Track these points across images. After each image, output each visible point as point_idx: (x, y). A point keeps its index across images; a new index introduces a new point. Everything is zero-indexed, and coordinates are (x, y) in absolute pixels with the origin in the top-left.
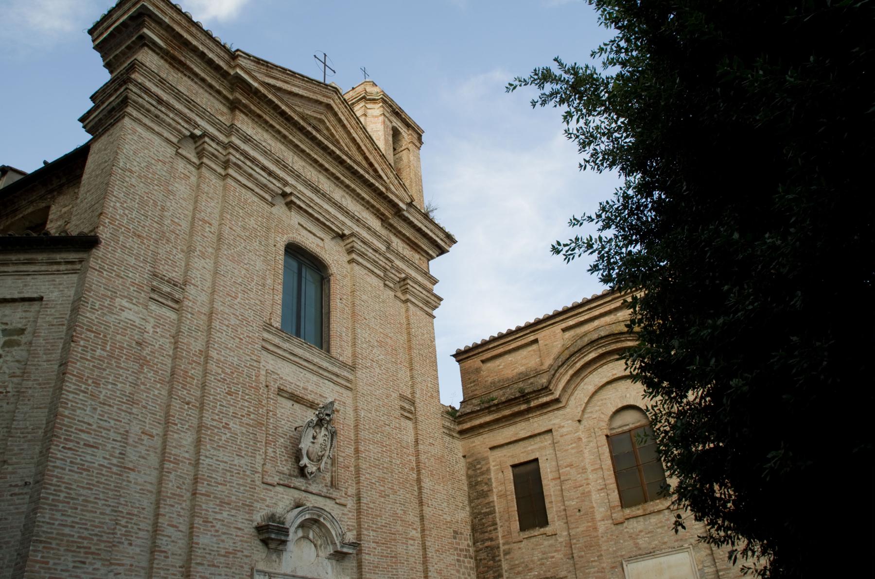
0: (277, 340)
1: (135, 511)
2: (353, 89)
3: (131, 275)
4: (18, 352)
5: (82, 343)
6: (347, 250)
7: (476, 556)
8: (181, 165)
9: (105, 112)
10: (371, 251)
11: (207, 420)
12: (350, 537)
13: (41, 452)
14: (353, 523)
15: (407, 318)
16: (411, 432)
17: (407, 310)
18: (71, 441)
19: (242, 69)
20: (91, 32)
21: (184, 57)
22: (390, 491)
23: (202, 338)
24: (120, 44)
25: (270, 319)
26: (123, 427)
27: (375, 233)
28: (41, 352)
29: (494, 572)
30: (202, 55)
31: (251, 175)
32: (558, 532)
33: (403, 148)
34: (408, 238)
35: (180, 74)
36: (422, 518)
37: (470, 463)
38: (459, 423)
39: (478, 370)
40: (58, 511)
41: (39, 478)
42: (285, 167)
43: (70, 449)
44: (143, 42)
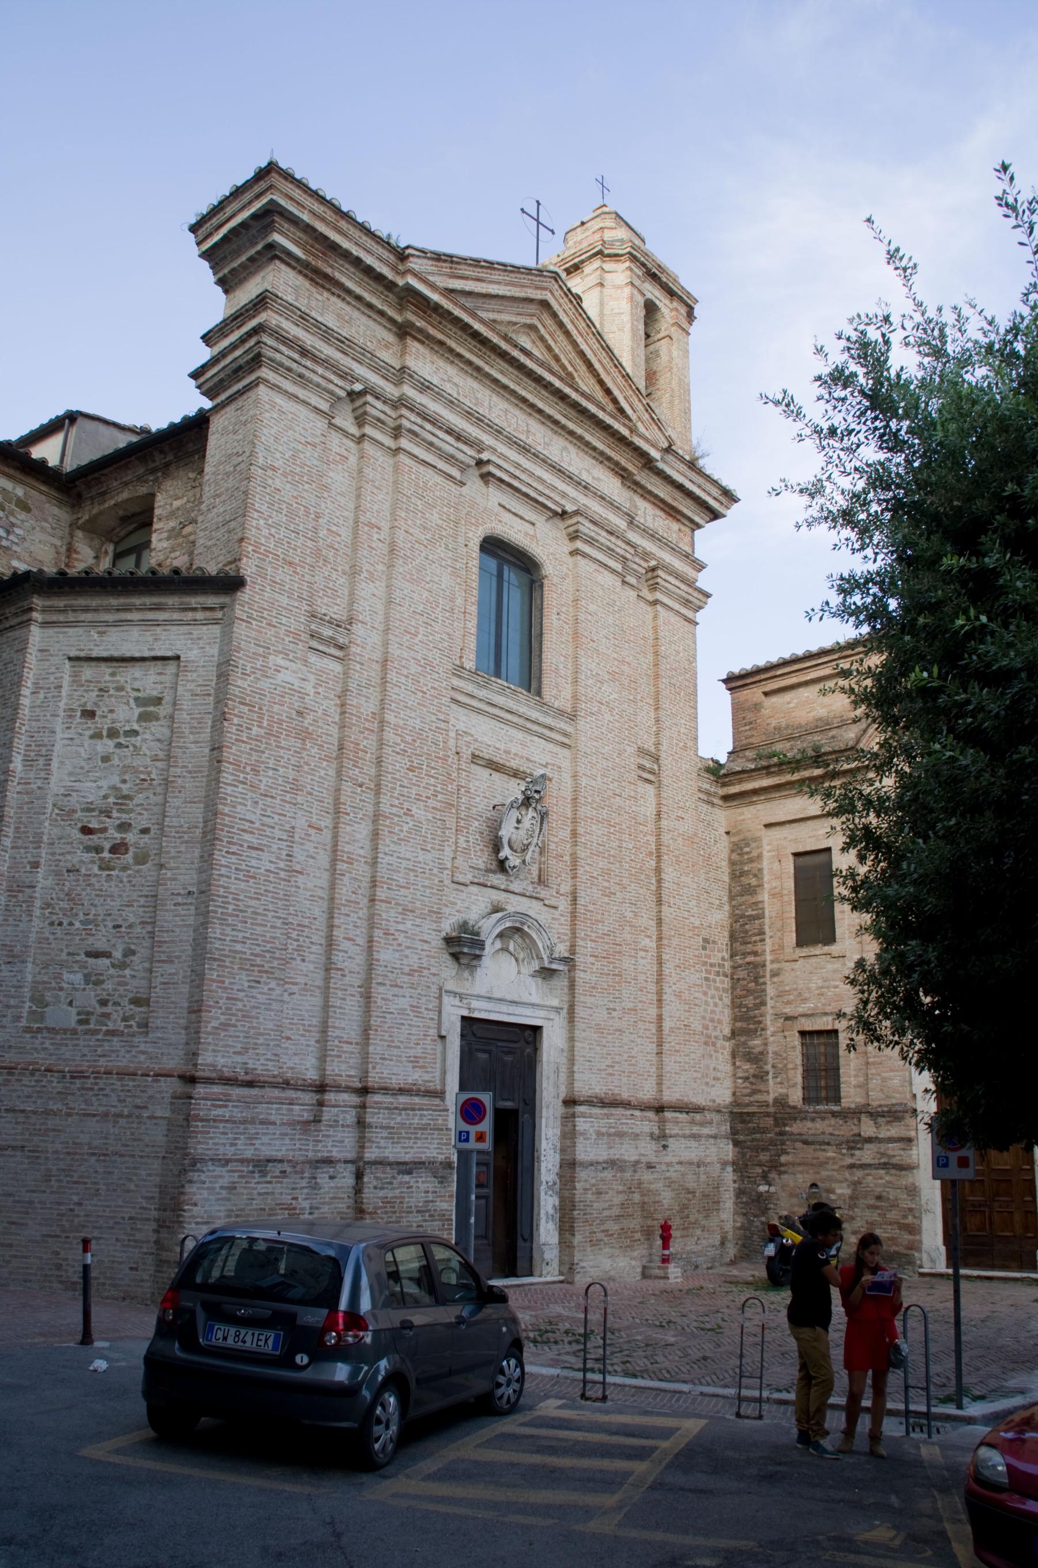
0: (470, 688)
1: (306, 922)
2: (583, 224)
3: (284, 620)
4: (159, 728)
5: (236, 721)
6: (569, 535)
7: (732, 974)
8: (335, 440)
9: (228, 371)
10: (604, 534)
11: (385, 808)
12: (562, 950)
13: (202, 857)
14: (566, 930)
15: (655, 629)
16: (652, 802)
17: (655, 617)
18: (234, 844)
19: (416, 275)
20: (194, 229)
21: (332, 267)
22: (618, 887)
23: (374, 694)
24: (238, 253)
25: (461, 657)
26: (288, 822)
27: (612, 505)
28: (187, 731)
29: (755, 998)
30: (357, 262)
31: (431, 444)
32: (848, 954)
33: (660, 336)
34: (662, 501)
35: (326, 294)
36: (660, 922)
37: (735, 844)
38: (724, 785)
39: (757, 707)
40: (228, 925)
41: (203, 887)
42: (479, 420)
43: (233, 853)
44: (273, 253)
